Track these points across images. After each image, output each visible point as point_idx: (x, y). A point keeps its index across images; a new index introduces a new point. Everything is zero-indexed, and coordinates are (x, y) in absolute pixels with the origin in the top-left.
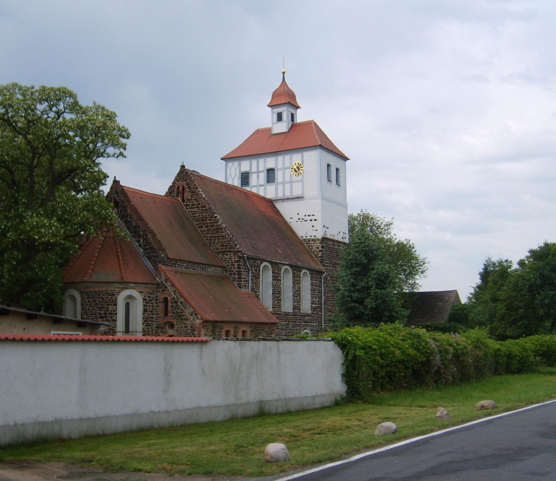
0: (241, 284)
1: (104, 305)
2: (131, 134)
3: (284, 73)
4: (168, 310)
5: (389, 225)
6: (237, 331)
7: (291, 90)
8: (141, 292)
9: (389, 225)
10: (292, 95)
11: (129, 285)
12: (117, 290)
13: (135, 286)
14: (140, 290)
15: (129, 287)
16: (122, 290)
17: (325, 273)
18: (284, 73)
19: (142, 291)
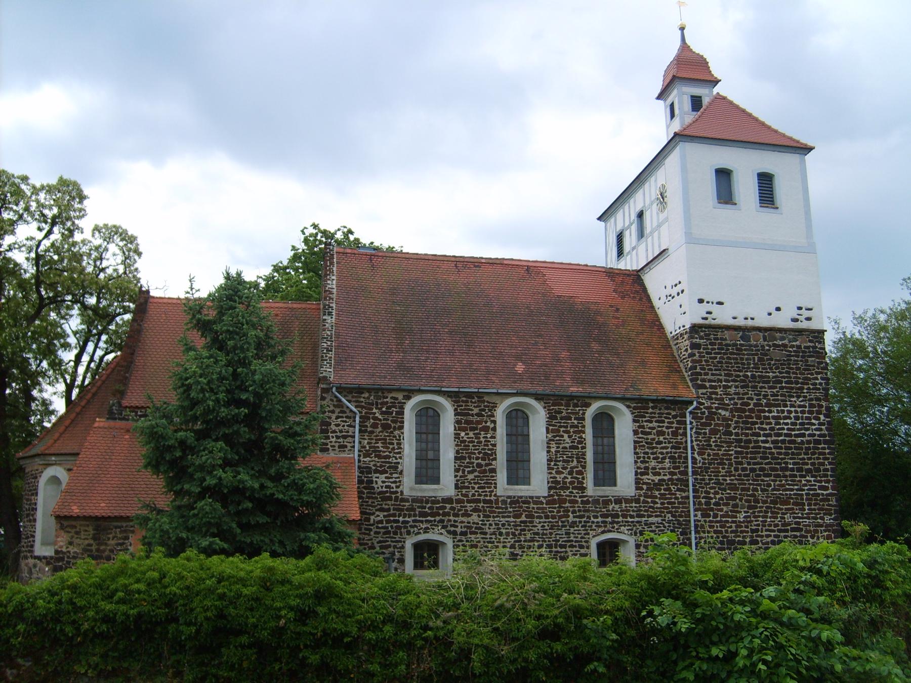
0: (327, 444)
1: (469, 446)
2: (135, 235)
3: (682, 29)
4: (40, 313)
5: (146, 467)
6: (178, 494)
7: (698, 54)
8: (69, 470)
9: (146, 467)
10: (702, 63)
11: (48, 458)
12: (40, 468)
13: (57, 459)
14: (68, 467)
15: (50, 462)
16: (45, 469)
17: (695, 403)
18: (682, 29)
19: (72, 467)
